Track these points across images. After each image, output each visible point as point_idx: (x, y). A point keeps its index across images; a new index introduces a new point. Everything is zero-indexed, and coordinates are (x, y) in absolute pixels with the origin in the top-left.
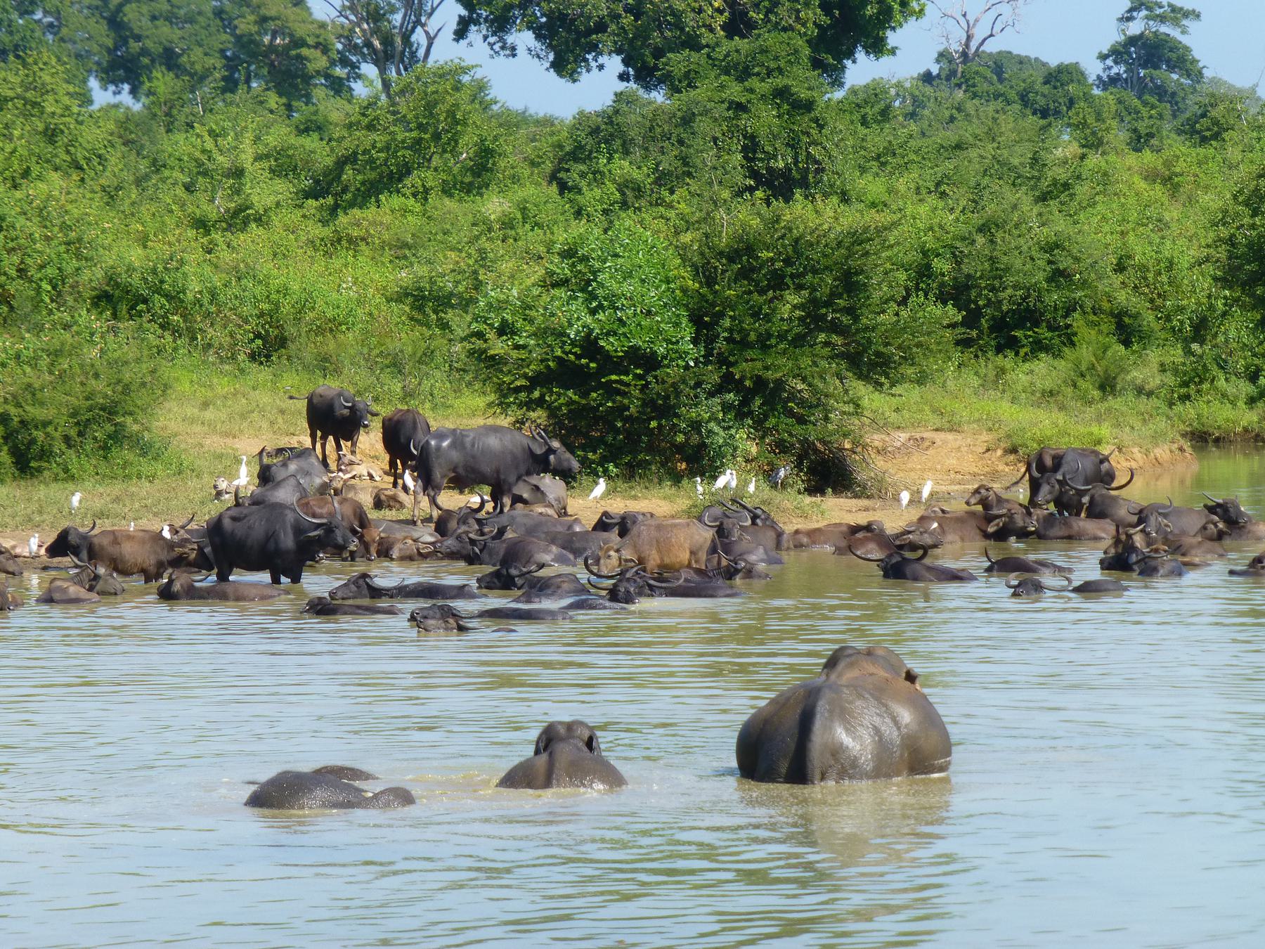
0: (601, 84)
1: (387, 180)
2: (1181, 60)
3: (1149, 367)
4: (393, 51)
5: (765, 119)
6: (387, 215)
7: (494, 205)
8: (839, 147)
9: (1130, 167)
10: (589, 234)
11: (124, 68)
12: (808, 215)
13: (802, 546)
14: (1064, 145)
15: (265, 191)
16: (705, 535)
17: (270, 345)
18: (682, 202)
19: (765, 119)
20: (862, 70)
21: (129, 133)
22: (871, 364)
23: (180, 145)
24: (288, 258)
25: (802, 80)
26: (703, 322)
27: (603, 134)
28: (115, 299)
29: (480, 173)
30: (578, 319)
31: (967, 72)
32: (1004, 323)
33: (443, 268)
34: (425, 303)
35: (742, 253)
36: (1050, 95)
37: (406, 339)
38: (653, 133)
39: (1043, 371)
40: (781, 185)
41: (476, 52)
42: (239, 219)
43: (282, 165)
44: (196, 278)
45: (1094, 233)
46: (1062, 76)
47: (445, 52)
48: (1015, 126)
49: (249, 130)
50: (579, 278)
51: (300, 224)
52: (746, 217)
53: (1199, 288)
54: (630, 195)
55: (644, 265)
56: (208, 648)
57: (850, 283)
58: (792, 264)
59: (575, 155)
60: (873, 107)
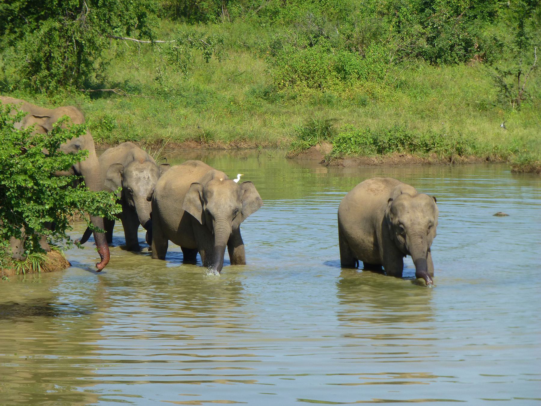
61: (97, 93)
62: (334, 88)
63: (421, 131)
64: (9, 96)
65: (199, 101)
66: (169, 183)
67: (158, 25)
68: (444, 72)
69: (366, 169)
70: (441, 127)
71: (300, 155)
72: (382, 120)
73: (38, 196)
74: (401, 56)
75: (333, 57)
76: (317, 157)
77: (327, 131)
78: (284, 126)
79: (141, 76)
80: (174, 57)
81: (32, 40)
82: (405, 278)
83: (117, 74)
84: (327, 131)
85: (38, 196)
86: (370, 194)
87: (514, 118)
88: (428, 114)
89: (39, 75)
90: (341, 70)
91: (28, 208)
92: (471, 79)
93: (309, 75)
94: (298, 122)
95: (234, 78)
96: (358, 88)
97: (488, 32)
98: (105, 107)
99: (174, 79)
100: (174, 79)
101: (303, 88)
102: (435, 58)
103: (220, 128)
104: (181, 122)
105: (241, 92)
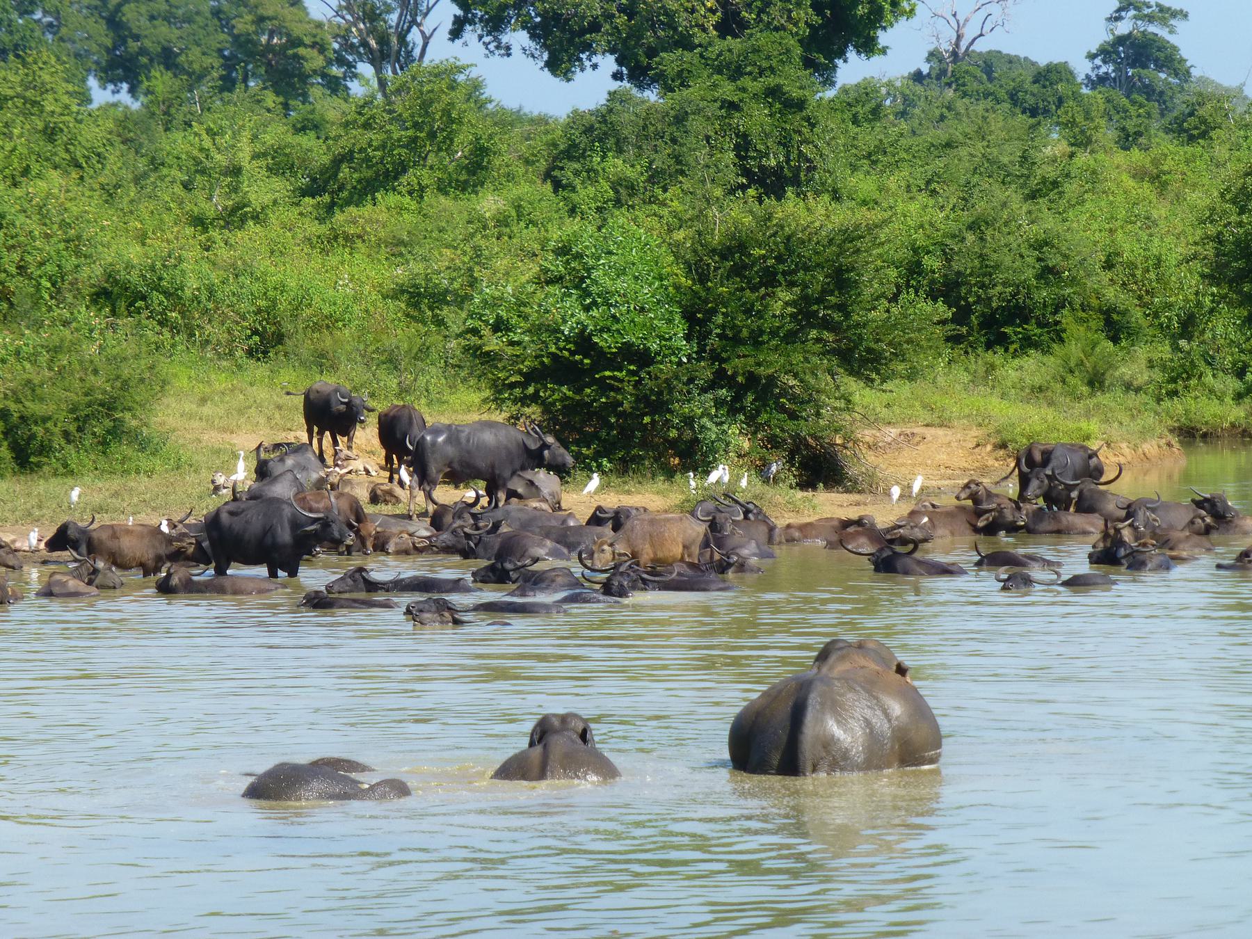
0: (595, 83)
1: (383, 178)
2: (1169, 60)
3: (1137, 363)
4: (389, 50)
5: (757, 118)
6: (383, 213)
7: (489, 203)
8: (830, 145)
9: (1119, 165)
10: (583, 232)
11: (123, 67)
12: (800, 213)
14: (1053, 144)
15: (262, 189)
16: (698, 529)
17: (267, 341)
18: (675, 200)
19: (757, 118)
20: (853, 69)
21: (128, 132)
22: (862, 360)
23: (178, 143)
24: (285, 256)
25: (793, 79)
26: (696, 318)
27: (597, 133)
28: (113, 295)
29: (475, 171)
30: (572, 316)
31: (957, 71)
32: (994, 319)
33: (438, 265)
34: (421, 300)
35: (734, 250)
36: (1039, 94)
37: (402, 336)
38: (647, 131)
39: (1032, 367)
40: (773, 183)
41: (471, 51)
42: (236, 216)
43: (280, 163)
44: (194, 276)
45: (1083, 230)
46: (1051, 75)
47: (441, 51)
48: (1004, 124)
49: (247, 129)
50: (573, 275)
51: (297, 222)
52: (738, 215)
53: (1187, 285)
54: (624, 193)
55: (637, 262)
57: (842, 280)
58: (783, 262)
59: (570, 153)
60: (864, 106)
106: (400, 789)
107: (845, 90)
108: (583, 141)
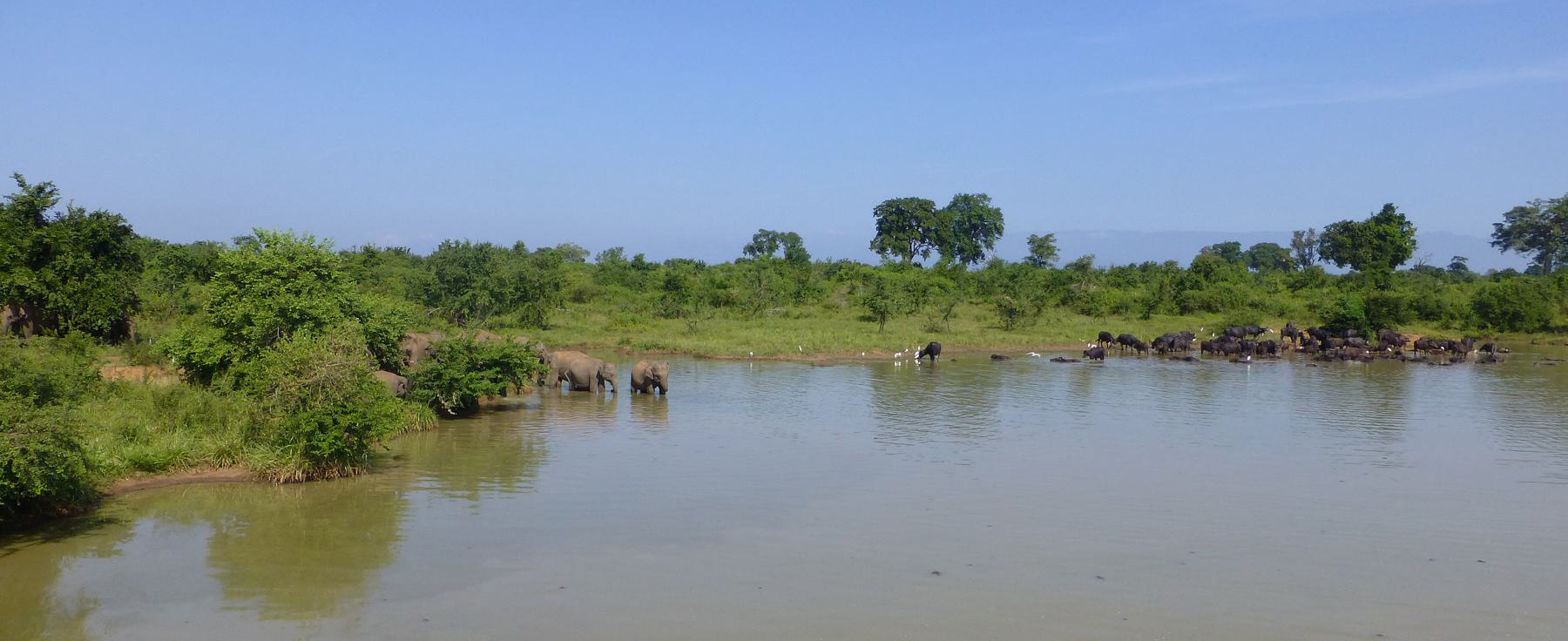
0: (1347, 269)
1: (1304, 285)
2: (1464, 268)
3: (1457, 324)
4: (1305, 262)
5: (1379, 276)
6: (1303, 292)
7: (1325, 290)
8: (1394, 282)
9: (1454, 287)
10: (1344, 296)
11: (1255, 265)
12: (1387, 293)
13: (728, 302)
14: (1440, 283)
15: (1281, 287)
16: (955, 309)
17: (1281, 314)
18: (1363, 290)
19: (1379, 276)
20: (1399, 268)
21: (1257, 277)
22: (1401, 322)
23: (1265, 279)
24: (1284, 298)
25: (1387, 269)
26: (1367, 312)
27: (1347, 278)
28: (1253, 305)
29: (1323, 283)
30: (1342, 311)
31: (1419, 269)
32: (1427, 314)
33: (1316, 301)
34: (1311, 307)
35: (1375, 300)
36: (1437, 273)
37: (1308, 314)
38: (1358, 278)
39: (1435, 324)
40: (1383, 288)
41: (1323, 262)
42: (1276, 291)
43: (1285, 282)
44: (1268, 302)
45: (1446, 299)
46: (1440, 270)
47: (1316, 263)
48: (1429, 278)
49: (1279, 277)
50: (1343, 304)
51: (1289, 293)
52: (1375, 294)
53: (1468, 310)
54: (1352, 289)
55: (1355, 302)
56: (427, 485)
57: (1397, 306)
58: (1386, 303)
59: (1341, 282)
60: (1401, 275)
61: (545, 328)
62: (631, 326)
63: (662, 342)
64: (726, 317)
65: (582, 331)
66: (581, 363)
67: (567, 304)
68: (670, 322)
69: (642, 355)
70: (668, 341)
71: (618, 350)
72: (646, 339)
73: (521, 366)
74: (655, 316)
75: (630, 316)
76: (624, 350)
77: (628, 342)
78: (612, 340)
79: (561, 322)
80: (573, 316)
81: (522, 310)
82: (1557, 328)
83: (552, 322)
84: (628, 342)
85: (521, 366)
86: (642, 366)
87: (694, 338)
88: (664, 336)
89: (524, 322)
90: (634, 321)
91: (518, 370)
92: (678, 324)
93: (622, 322)
94: (618, 339)
95: (595, 323)
96: (640, 326)
97: (685, 307)
98: (548, 333)
99: (573, 323)
100: (573, 323)
101: (620, 327)
102: (666, 316)
103: (589, 341)
104: (575, 339)
105: (597, 328)
106: (17, 176)
107: (995, 265)
108: (1137, 275)
